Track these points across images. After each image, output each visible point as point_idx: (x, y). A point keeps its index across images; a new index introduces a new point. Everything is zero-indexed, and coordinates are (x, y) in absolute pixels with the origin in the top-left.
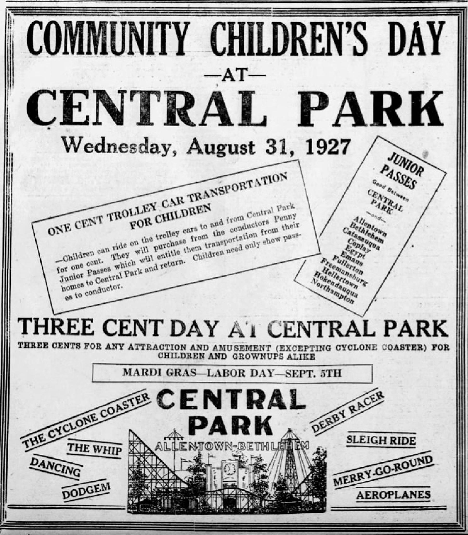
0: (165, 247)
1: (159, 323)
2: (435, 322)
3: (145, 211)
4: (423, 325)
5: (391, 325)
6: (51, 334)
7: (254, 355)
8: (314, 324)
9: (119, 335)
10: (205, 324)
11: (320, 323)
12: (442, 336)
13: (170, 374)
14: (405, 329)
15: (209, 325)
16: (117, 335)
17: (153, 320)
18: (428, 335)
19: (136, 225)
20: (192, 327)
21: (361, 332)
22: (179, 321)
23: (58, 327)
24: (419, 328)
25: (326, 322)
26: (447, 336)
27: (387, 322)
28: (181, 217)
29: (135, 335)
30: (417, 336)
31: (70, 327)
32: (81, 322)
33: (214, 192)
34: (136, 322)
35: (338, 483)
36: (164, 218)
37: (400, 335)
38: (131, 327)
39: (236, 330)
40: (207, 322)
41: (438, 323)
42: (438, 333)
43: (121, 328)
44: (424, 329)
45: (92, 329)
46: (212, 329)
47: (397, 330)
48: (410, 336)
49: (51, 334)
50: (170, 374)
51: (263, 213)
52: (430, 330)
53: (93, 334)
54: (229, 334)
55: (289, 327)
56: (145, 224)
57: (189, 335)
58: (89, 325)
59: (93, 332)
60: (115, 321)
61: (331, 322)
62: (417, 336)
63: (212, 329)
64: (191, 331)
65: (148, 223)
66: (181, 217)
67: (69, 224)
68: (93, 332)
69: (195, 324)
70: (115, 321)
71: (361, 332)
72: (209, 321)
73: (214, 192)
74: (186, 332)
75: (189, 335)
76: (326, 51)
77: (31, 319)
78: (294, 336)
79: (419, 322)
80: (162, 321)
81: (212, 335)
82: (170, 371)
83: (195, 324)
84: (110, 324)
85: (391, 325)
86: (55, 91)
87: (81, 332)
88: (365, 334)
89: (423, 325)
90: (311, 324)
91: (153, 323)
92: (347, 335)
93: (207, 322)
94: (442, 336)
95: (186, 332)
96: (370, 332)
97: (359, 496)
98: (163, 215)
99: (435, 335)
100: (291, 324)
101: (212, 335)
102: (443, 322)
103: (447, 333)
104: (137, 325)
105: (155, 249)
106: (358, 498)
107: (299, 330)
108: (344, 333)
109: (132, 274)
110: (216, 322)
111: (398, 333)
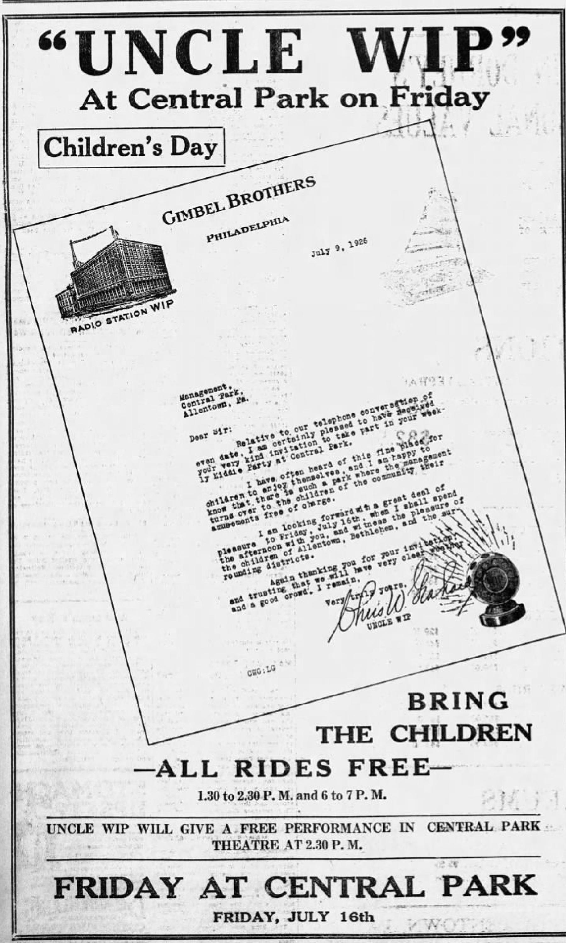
1: (241, 882)
2: (517, 877)
3: (87, 832)
4: (244, 765)
5: (453, 882)
9: (290, 896)
11: (344, 880)
13: (185, 831)
16: (286, 897)
17: (321, 728)
19: (320, 828)
21: (404, 891)
25: (353, 879)
28: (84, 832)
33: (367, 827)
37: (467, 894)
41: (522, 879)
42: (522, 890)
44: (88, 889)
45: (298, 54)
46: (171, 888)
50: (185, 831)
51: (200, 101)
52: (511, 887)
55: (285, 45)
56: (330, 830)
57: (138, 896)
60: (284, 880)
63: (171, 888)
64: (141, 890)
65: (335, 830)
66: (84, 832)
67: (277, 841)
70: (284, 880)
71: (404, 891)
73: (367, 827)
74: (135, 892)
75: (138, 896)
77: (353, 879)
79: (494, 878)
80: (245, 879)
82: (185, 827)
86: (285, 878)
88: (410, 894)
91: (339, 882)
95: (135, 892)
100: (302, 881)
102: (529, 876)
103: (536, 890)
111: (465, 892)
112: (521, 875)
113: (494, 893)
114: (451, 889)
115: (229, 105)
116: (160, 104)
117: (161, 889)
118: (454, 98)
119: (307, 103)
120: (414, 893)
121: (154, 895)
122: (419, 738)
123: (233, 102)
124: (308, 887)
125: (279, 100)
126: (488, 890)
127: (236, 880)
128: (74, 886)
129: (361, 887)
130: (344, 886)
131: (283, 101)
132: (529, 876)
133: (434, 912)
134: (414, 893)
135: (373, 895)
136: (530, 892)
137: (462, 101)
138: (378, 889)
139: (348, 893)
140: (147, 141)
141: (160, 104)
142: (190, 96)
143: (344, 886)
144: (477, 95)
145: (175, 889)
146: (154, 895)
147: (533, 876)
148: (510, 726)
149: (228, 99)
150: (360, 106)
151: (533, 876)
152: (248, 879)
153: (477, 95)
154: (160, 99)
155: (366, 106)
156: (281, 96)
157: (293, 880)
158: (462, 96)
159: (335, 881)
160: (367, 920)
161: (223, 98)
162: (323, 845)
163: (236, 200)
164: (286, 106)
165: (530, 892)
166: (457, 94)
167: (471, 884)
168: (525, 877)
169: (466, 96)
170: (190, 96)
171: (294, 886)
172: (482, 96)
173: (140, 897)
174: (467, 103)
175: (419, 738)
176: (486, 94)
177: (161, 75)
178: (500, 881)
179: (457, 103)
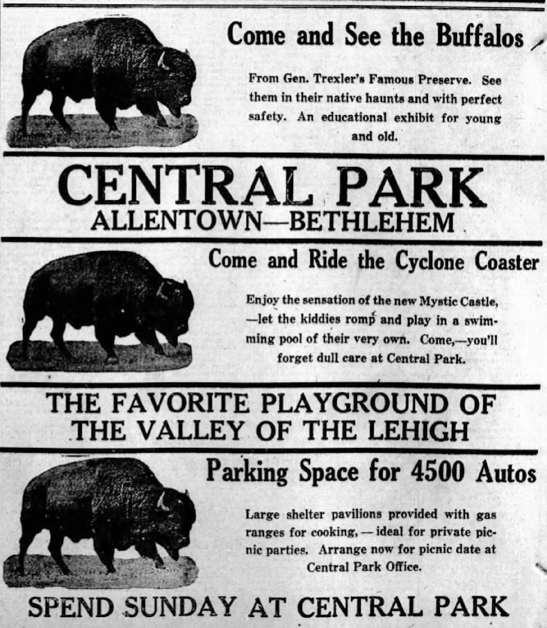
0: (330, 553)
1: (281, 602)
2: (494, 598)
7: (226, 216)
8: (352, 600)
10: (220, 601)
11: (359, 599)
14: (387, 188)
15: (224, 602)
18: (485, 614)
20: (457, 604)
21: (407, 610)
25: (366, 598)
27: (438, 598)
29: (80, 616)
30: (473, 615)
34: (336, 600)
37: (454, 614)
38: (330, 607)
39: (257, 608)
41: (497, 600)
43: (319, 607)
46: (228, 606)
47: (450, 609)
48: (262, 616)
51: (333, 568)
52: (488, 607)
53: (248, 411)
55: (67, 604)
57: (201, 614)
60: (312, 600)
61: (372, 598)
62: (473, 615)
63: (228, 606)
64: (203, 609)
69: (207, 600)
70: (312, 600)
71: (407, 610)
72: (225, 597)
75: (201, 614)
76: (332, 614)
79: (475, 598)
80: (284, 600)
81: (236, 438)
83: (207, 600)
84: (307, 603)
85: (443, 602)
88: (411, 614)
89: (480, 602)
90: (349, 600)
91: (355, 601)
93: (223, 599)
96: (416, 610)
97: (96, 223)
99: (494, 614)
101: (236, 438)
102: (503, 598)
105: (268, 553)
106: (94, 228)
107: (335, 606)
109: (365, 568)
110: (233, 598)
113: (475, 614)
117: (219, 608)
118: (463, 550)
119: (373, 568)
121: (213, 613)
126: (470, 610)
127: (277, 600)
129: (372, 606)
132: (503, 598)
133: (422, 21)
135: (382, 614)
136: (504, 614)
138: (386, 608)
144: (426, 319)
145: (231, 608)
146: (213, 613)
149: (398, 531)
152: (287, 601)
157: (320, 599)
163: (299, 220)
165: (504, 614)
167: (97, 220)
173: (202, 615)
174: (423, 323)
176: (378, 337)
177: (263, 166)
178: (480, 602)
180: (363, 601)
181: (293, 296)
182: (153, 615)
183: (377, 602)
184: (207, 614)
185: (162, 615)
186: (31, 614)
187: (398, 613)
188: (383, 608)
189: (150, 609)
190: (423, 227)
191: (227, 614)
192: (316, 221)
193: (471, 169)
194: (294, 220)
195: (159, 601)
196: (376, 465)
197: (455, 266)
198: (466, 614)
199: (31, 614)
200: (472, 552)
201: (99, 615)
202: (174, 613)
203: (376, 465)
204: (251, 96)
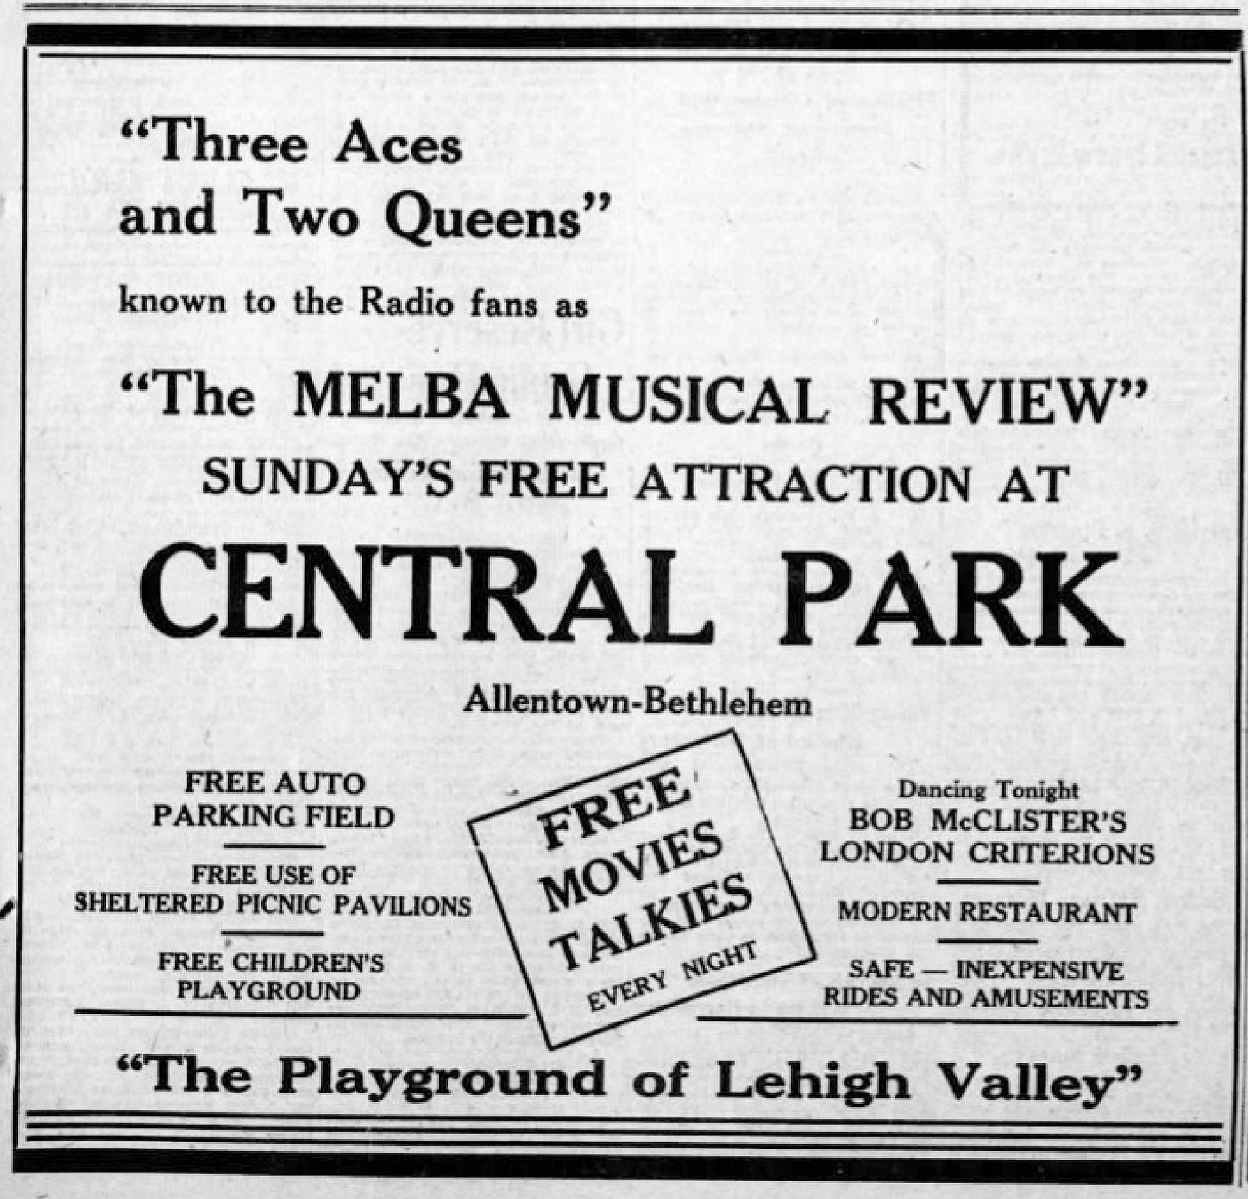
1: (1061, 474)
5: (818, 577)
6: (350, 415)
7: (1078, 390)
9: (226, 633)
11: (421, 558)
12: (1091, 642)
14: (897, 602)
22: (899, 844)
23: (994, 602)
24: (967, 596)
25: (453, 555)
26: (1119, 642)
27: (157, 808)
31: (553, 479)
32: (577, 469)
35: (944, 824)
36: (254, 962)
40: (387, 465)
41: (1067, 572)
44: (994, 602)
46: (396, 479)
49: (350, 415)
52: (1026, 607)
53: (604, 494)
54: (636, 492)
55: (253, 577)
57: (346, 492)
58: (267, 582)
59: (947, 415)
60: (208, 556)
63: (396, 479)
64: (350, 482)
68: (947, 415)
69: (358, 466)
70: (208, 556)
71: (639, 617)
75: (346, 492)
76: (298, 623)
77: (453, 555)
78: (284, 630)
83: (358, 466)
84: (179, 570)
85: (818, 577)
87: (578, 491)
88: (660, 633)
91: (404, 564)
92: (562, 634)
93: (387, 465)
94: (1091, 642)
98: (254, 955)
99: (1051, 636)
102: (1096, 560)
103: (1116, 629)
104: (358, 591)
108: (546, 622)
112: (1061, 557)
114: (811, 608)
115: (1006, 1094)
116: (770, 1089)
117: (382, 482)
120: (675, 628)
122: (259, 966)
123: (1014, 1089)
124: (1099, 1000)
125: (985, 1085)
126: (946, 625)
128: (508, 475)
129: (750, 482)
130: (1127, 999)
131: (348, 1080)
134: (675, 628)
135: (768, 497)
137: (350, 1085)
138: (775, 487)
139: (434, 626)
140: (585, 203)
141: (770, 1089)
142: (671, 1075)
143: (1127, 999)
144: (377, 1074)
146: (370, 491)
147: (1112, 557)
148: (279, 552)
149: (1004, 1083)
150: (671, 1095)
151: (1112, 557)
153: (377, 1074)
154: (771, 1080)
155: (547, 1093)
156: (989, 1079)
157: (238, 554)
158: (996, 1082)
159: (386, 561)
160: (703, 711)
161: (996, 1082)
162: (1001, 998)
164: (998, 1096)
166: (342, 1073)
168: (1084, 564)
169: (358, 1077)
170: (671, 1075)
171: (238, 588)
172: (1101, 1084)
175: (259, 966)
179: (341, 1088)
180: (732, 473)
181: (324, 293)
182: (258, 490)
183: (758, 475)
184: (358, 491)
185: (274, 491)
186: (207, 488)
187: (799, 495)
188: (770, 485)
189: (250, 480)
190: (684, 857)
191: (396, 491)
192: (258, 782)
193: (1088, 556)
194: (650, 699)
195: (269, 467)
196: (481, 296)
197: (434, 309)
198: (191, 823)
199: (207, 488)
200: (557, 711)
201: (311, 490)
202: (296, 490)
203: (481, 296)
204: (298, 298)
